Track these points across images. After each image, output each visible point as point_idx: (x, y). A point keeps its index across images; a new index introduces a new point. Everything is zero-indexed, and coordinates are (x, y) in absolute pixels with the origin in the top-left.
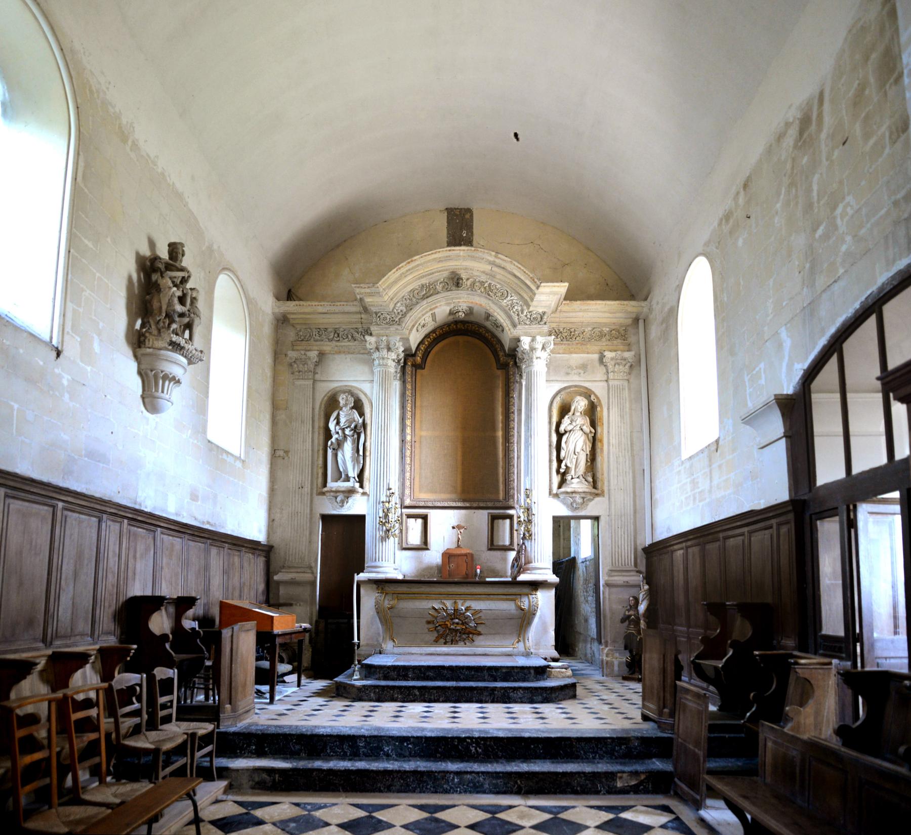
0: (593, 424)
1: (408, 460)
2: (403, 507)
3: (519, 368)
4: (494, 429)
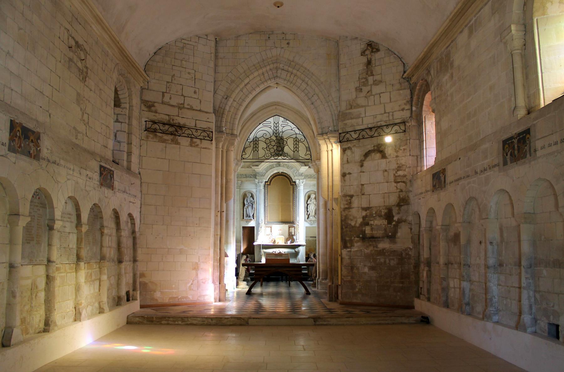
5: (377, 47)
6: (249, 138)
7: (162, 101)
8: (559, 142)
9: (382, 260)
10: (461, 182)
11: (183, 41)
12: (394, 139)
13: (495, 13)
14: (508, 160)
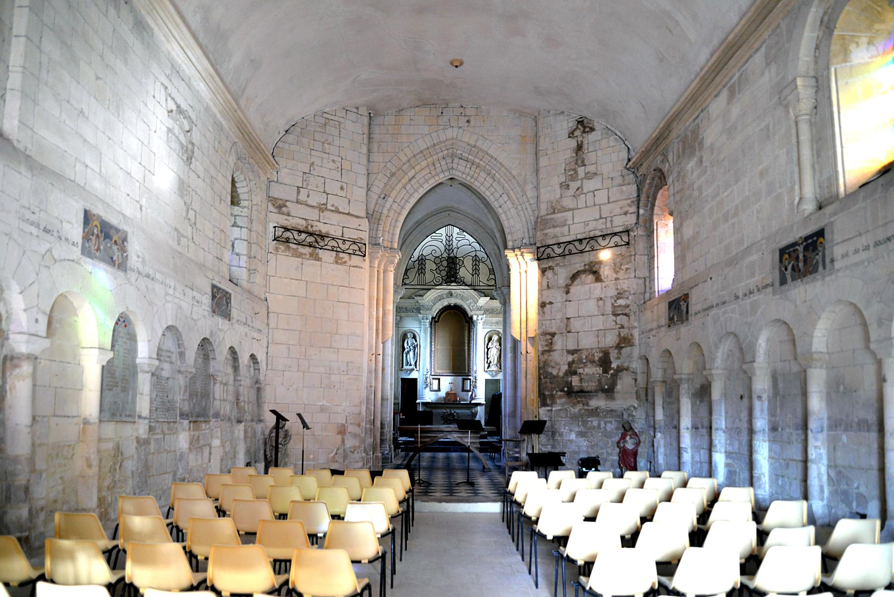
2: (431, 375)
4: (464, 346)
5: (590, 126)
7: (297, 199)
8: (871, 246)
9: (595, 424)
10: (714, 311)
11: (325, 115)
12: (613, 254)
13: (771, 62)
14: (789, 277)
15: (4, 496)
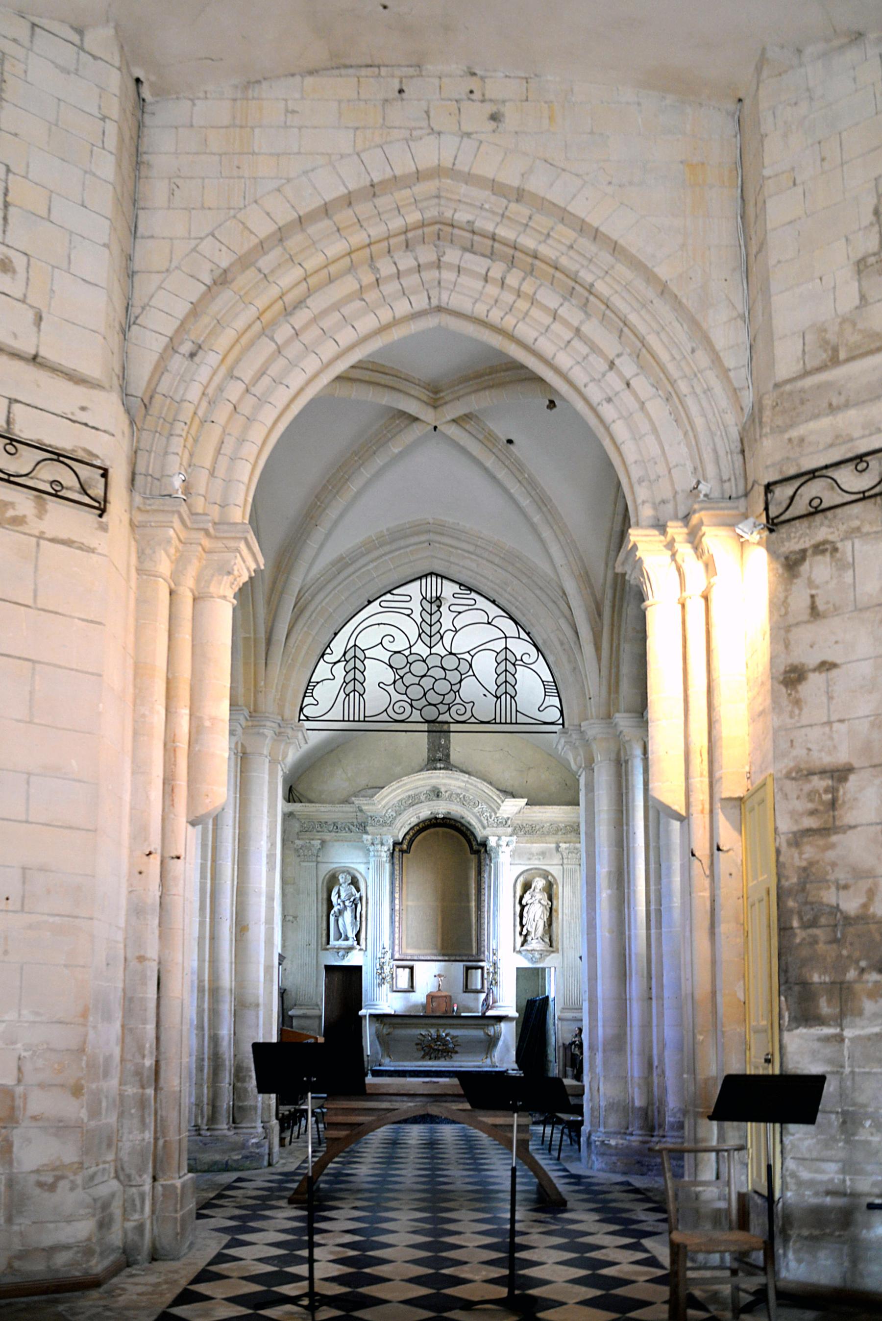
0: (550, 899)
1: (397, 924)
3: (489, 855)
4: (469, 901)
6: (328, 651)
15: (232, 1054)
